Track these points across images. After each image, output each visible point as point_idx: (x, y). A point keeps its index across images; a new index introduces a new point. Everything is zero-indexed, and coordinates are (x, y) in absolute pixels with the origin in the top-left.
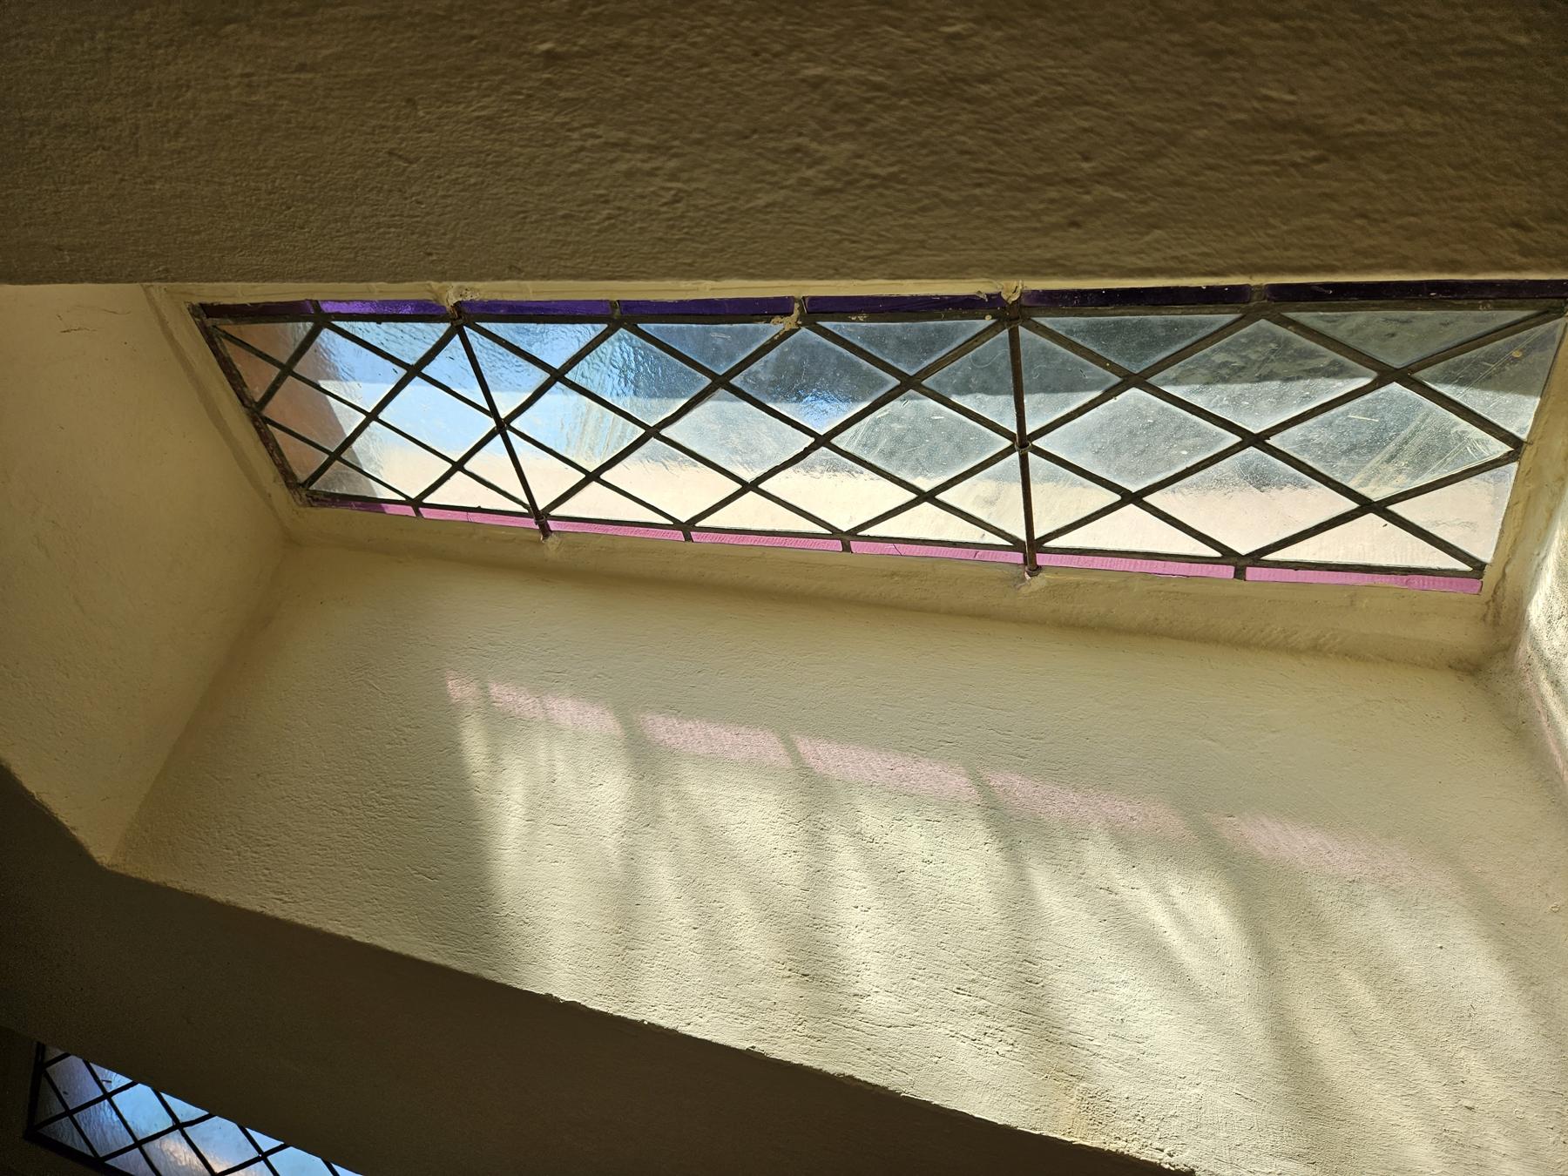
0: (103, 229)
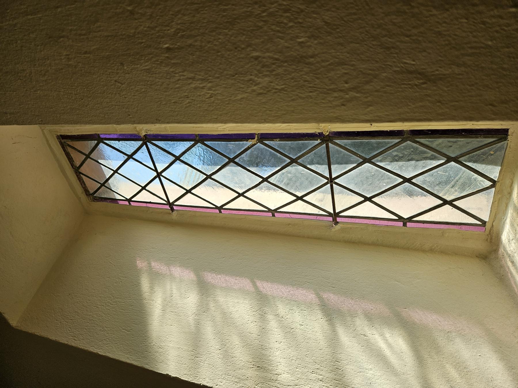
0: (20, 107)
